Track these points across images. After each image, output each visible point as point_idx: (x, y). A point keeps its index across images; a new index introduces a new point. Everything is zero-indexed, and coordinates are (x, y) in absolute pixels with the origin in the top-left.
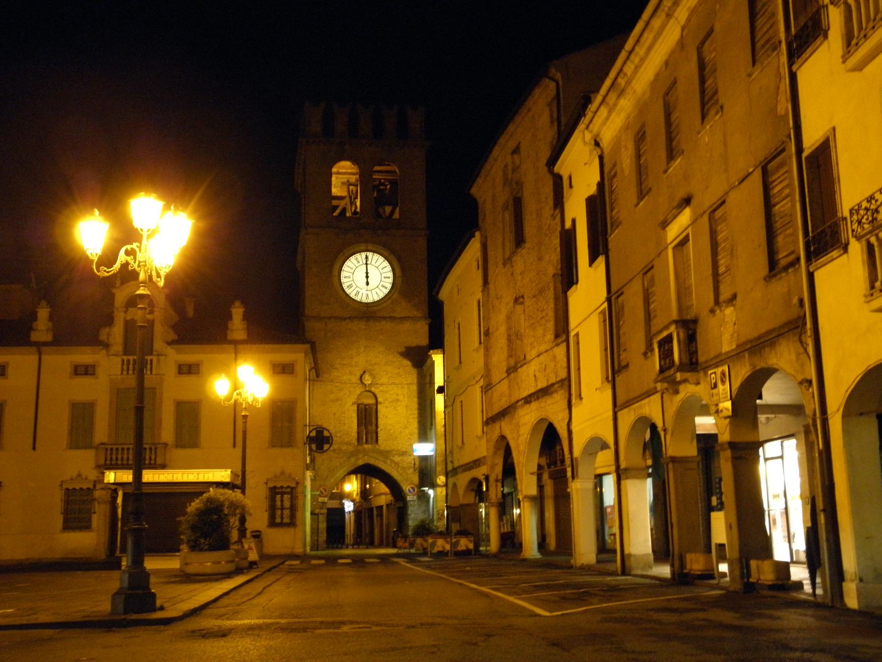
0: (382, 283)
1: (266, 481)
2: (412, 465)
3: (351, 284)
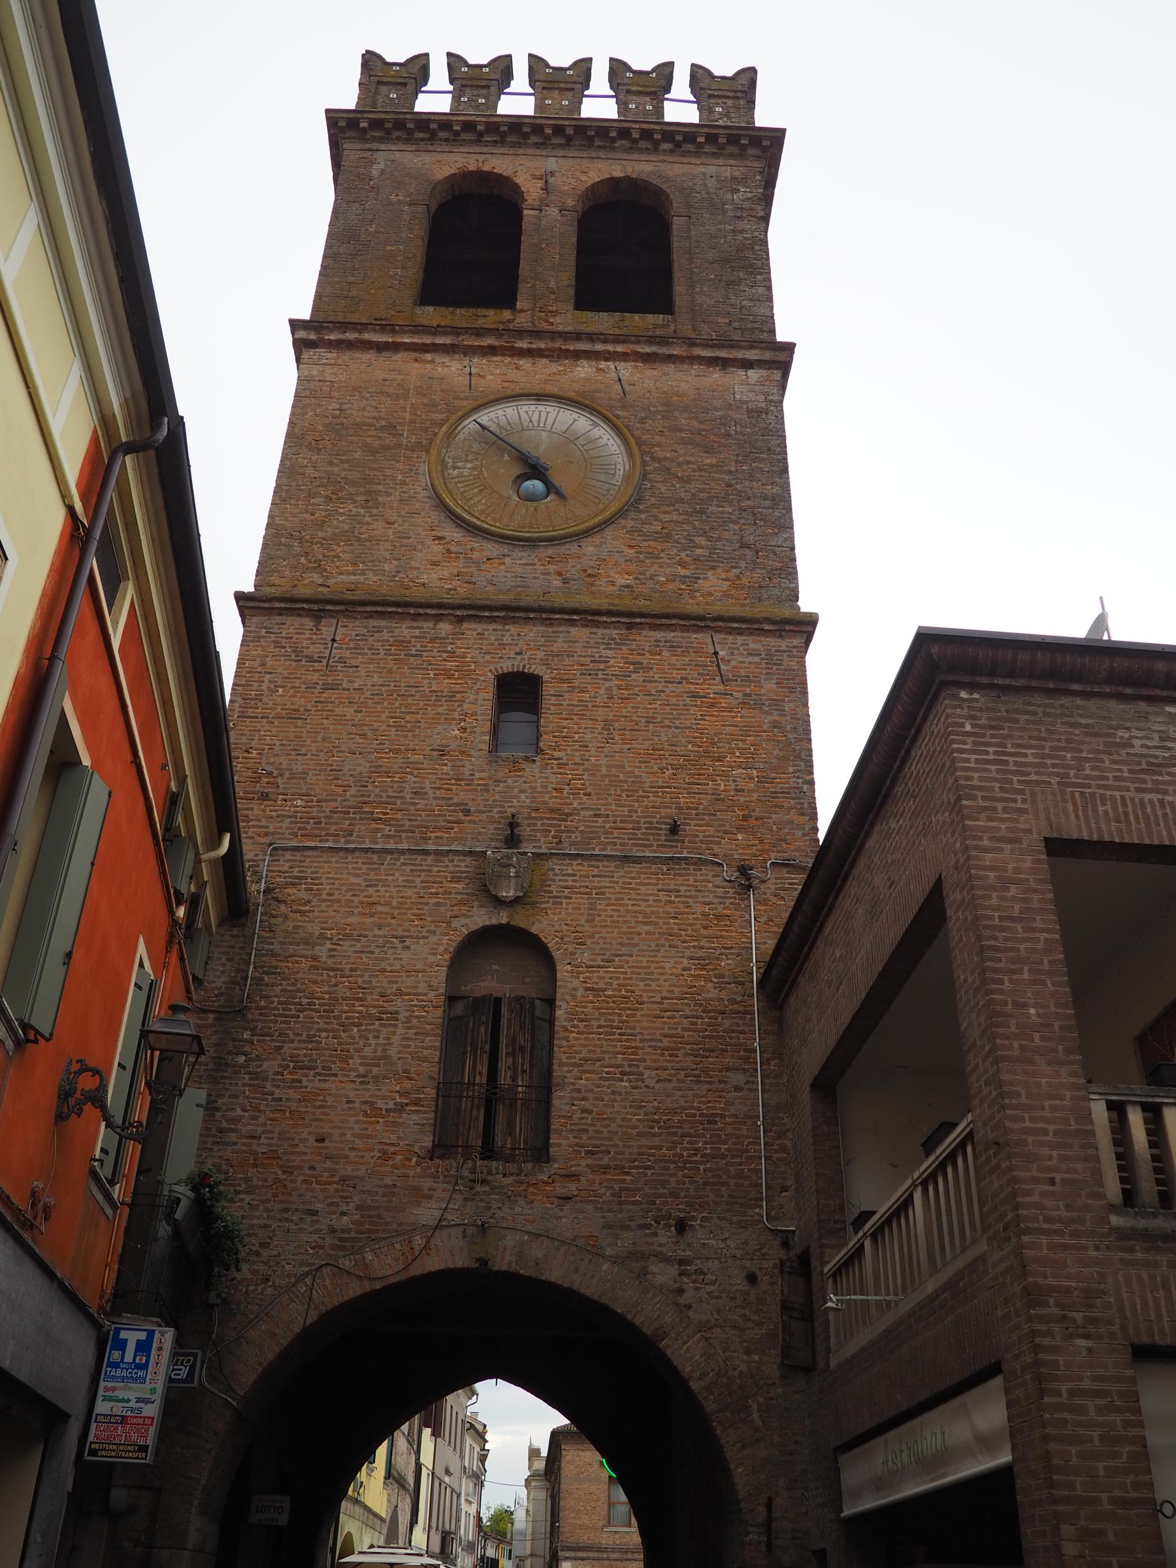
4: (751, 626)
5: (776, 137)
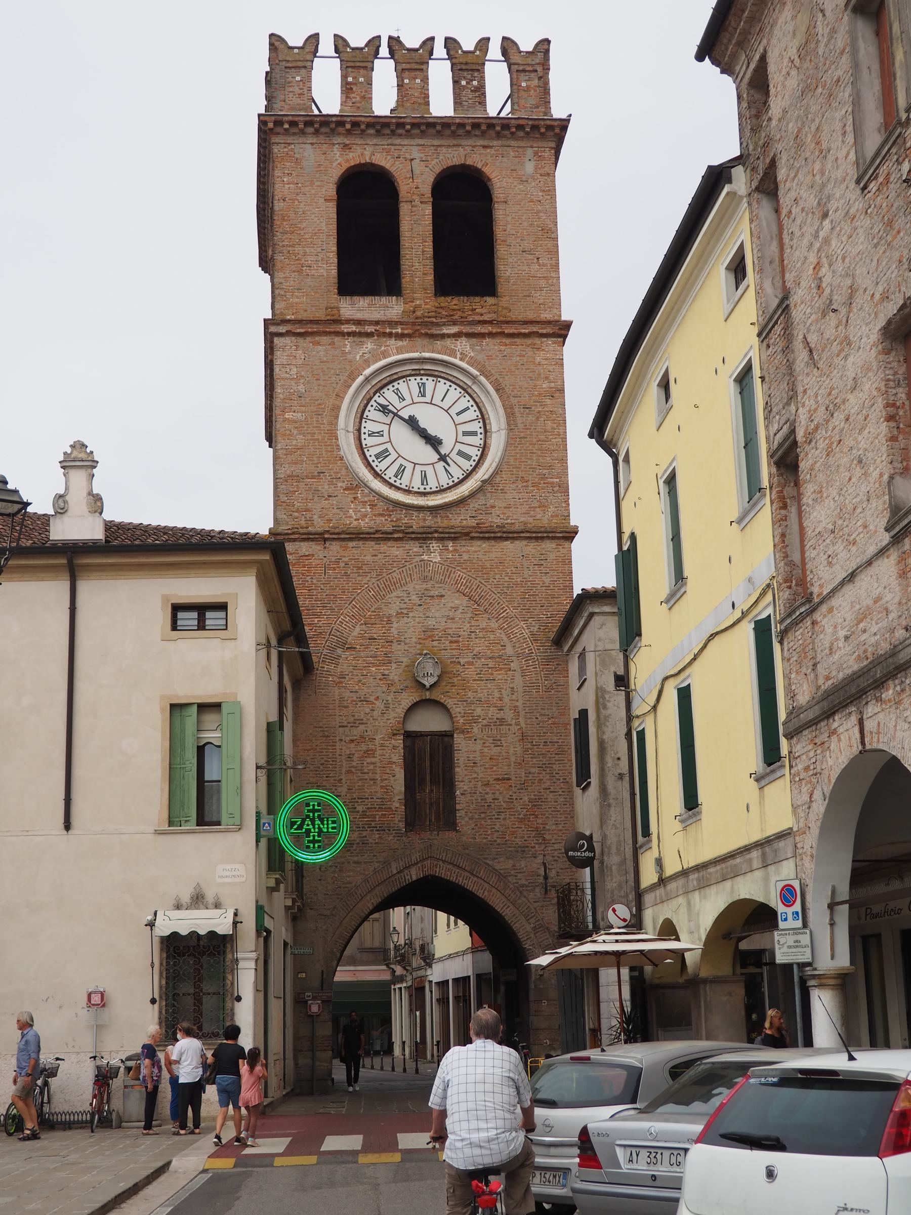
0: (459, 447)
1: (849, 1206)
2: (541, 880)
3: (386, 450)
4: (537, 535)
5: (563, 125)
